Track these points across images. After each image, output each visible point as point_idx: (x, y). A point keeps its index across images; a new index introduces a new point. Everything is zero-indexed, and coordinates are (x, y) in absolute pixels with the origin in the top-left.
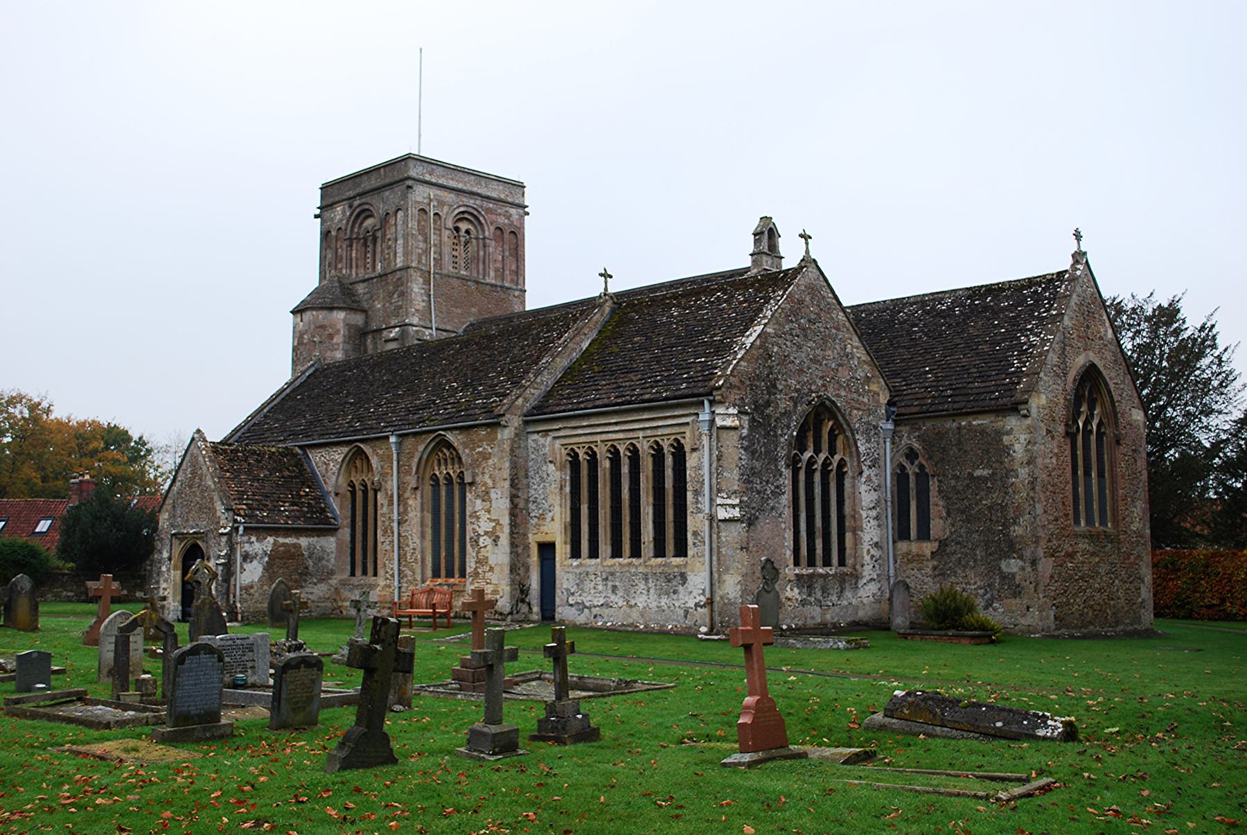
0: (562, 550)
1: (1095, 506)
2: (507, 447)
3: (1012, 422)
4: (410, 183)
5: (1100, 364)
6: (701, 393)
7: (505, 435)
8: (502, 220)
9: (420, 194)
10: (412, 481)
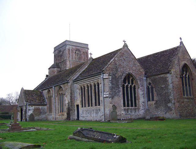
0: (80, 106)
1: (188, 92)
2: (70, 86)
3: (168, 75)
4: (66, 45)
5: (187, 64)
6: (102, 72)
7: (69, 84)
8: (84, 51)
9: (67, 47)
10: (56, 95)
